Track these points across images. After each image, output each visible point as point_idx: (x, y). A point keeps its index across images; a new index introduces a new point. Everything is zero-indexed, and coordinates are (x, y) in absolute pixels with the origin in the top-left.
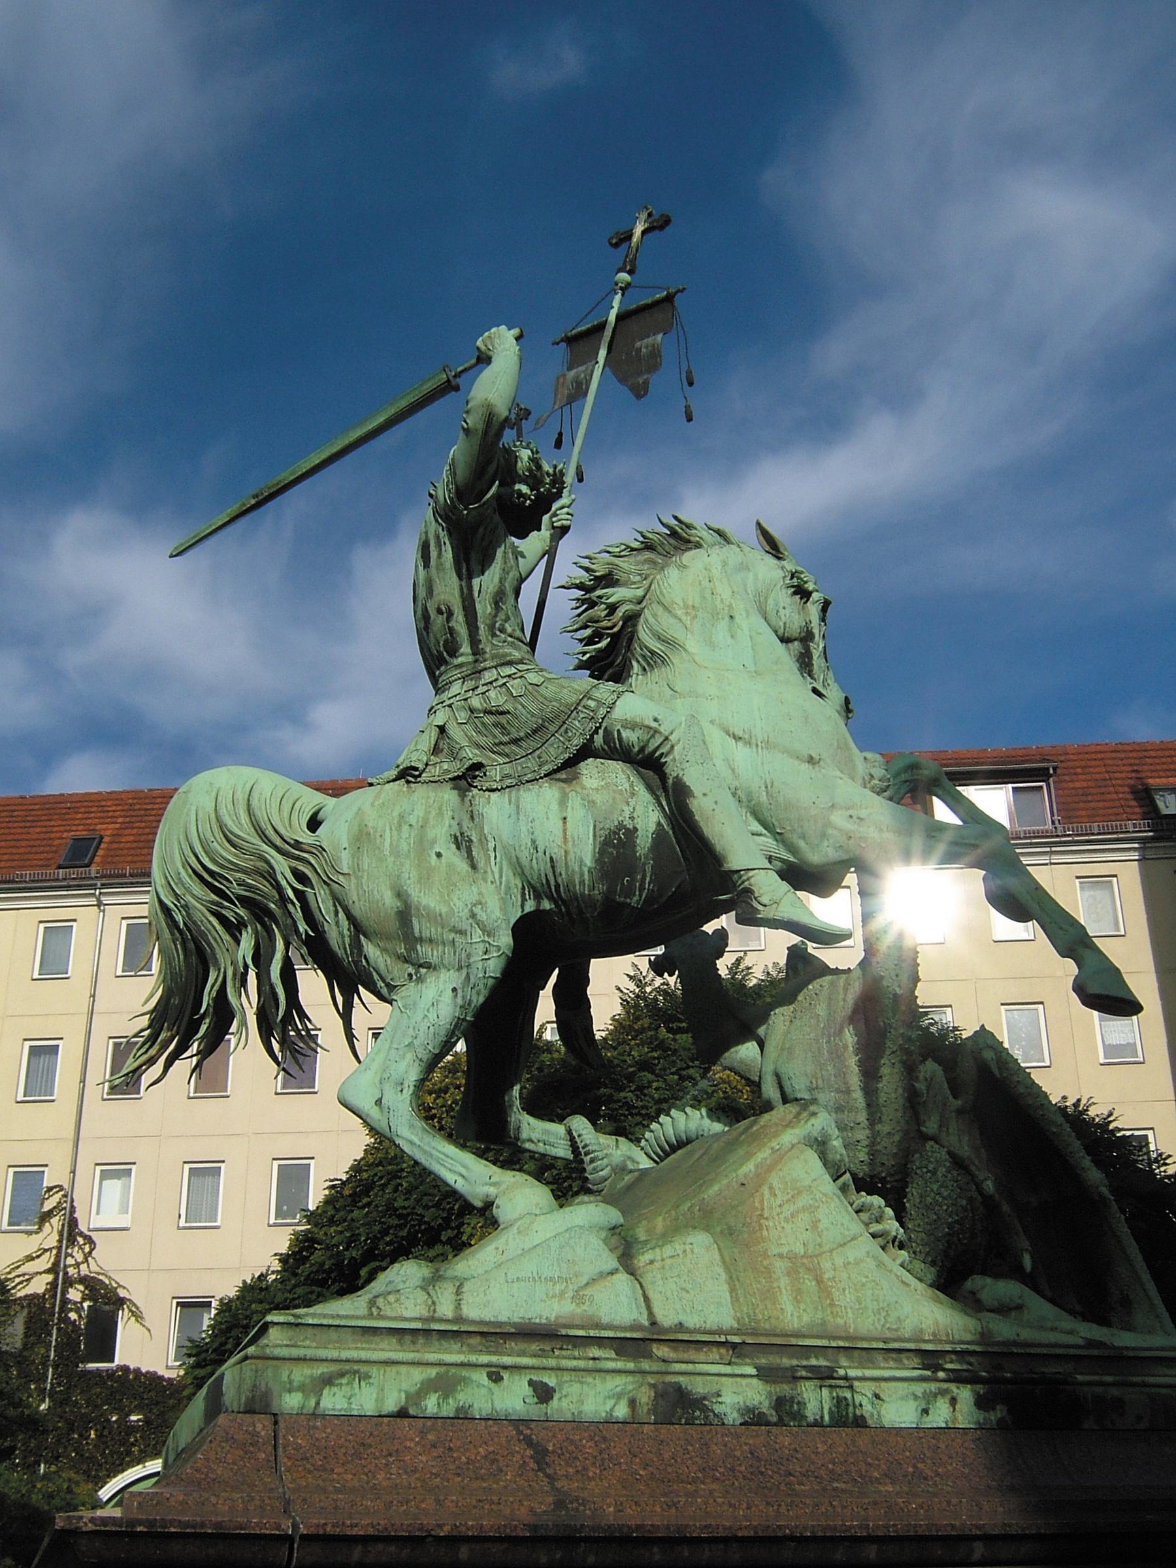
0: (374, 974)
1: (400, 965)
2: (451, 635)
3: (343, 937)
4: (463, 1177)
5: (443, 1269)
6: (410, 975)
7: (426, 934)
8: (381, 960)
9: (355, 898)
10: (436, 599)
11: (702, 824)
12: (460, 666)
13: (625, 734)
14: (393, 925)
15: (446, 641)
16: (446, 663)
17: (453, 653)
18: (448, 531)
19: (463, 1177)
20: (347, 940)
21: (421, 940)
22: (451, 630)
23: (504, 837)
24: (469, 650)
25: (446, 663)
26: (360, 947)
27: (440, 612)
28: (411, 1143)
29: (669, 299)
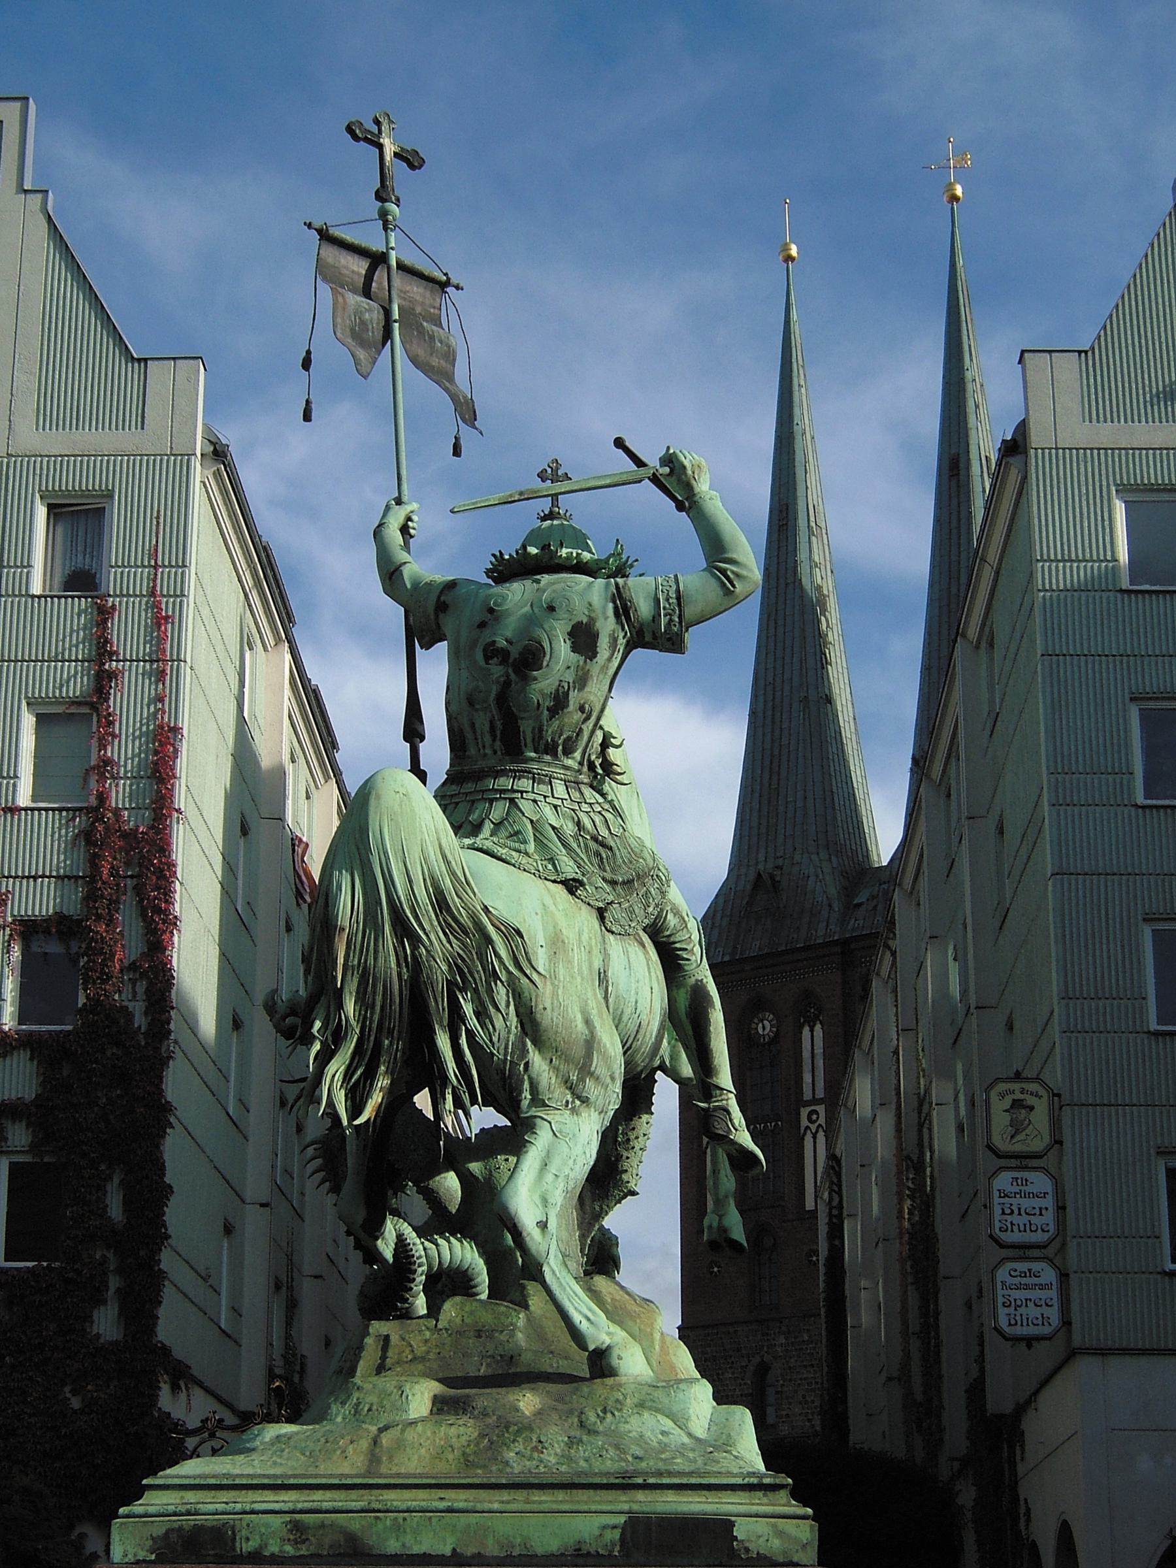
0: (526, 1085)
1: (563, 1089)
2: (578, 735)
3: (280, 970)
4: (588, 1319)
5: (408, 1386)
6: (567, 1102)
7: (598, 1072)
8: (546, 1074)
9: (548, 1005)
10: (584, 694)
11: (713, 1036)
12: (567, 768)
13: (670, 916)
14: (578, 1051)
15: (569, 738)
16: (555, 755)
17: (568, 752)
18: (628, 642)
19: (588, 1319)
20: (512, 1038)
21: (592, 1074)
22: (581, 730)
23: (620, 987)
24: (579, 758)
25: (555, 755)
26: (524, 1052)
27: (582, 709)
28: (554, 1272)
29: (443, 285)
